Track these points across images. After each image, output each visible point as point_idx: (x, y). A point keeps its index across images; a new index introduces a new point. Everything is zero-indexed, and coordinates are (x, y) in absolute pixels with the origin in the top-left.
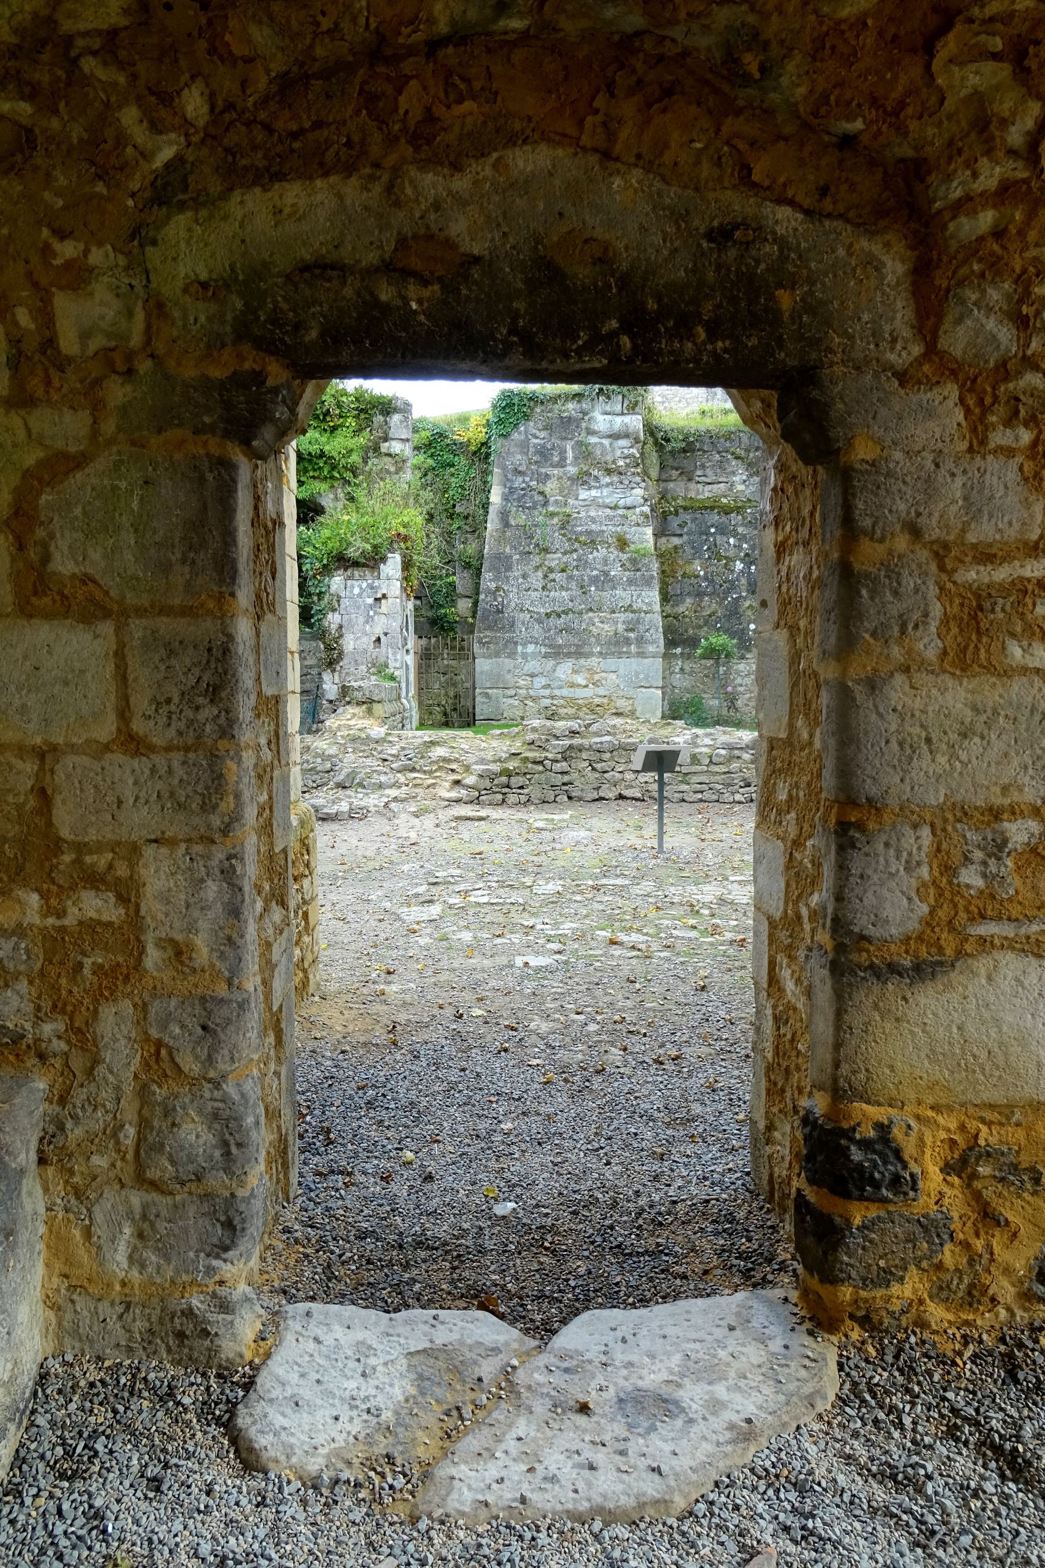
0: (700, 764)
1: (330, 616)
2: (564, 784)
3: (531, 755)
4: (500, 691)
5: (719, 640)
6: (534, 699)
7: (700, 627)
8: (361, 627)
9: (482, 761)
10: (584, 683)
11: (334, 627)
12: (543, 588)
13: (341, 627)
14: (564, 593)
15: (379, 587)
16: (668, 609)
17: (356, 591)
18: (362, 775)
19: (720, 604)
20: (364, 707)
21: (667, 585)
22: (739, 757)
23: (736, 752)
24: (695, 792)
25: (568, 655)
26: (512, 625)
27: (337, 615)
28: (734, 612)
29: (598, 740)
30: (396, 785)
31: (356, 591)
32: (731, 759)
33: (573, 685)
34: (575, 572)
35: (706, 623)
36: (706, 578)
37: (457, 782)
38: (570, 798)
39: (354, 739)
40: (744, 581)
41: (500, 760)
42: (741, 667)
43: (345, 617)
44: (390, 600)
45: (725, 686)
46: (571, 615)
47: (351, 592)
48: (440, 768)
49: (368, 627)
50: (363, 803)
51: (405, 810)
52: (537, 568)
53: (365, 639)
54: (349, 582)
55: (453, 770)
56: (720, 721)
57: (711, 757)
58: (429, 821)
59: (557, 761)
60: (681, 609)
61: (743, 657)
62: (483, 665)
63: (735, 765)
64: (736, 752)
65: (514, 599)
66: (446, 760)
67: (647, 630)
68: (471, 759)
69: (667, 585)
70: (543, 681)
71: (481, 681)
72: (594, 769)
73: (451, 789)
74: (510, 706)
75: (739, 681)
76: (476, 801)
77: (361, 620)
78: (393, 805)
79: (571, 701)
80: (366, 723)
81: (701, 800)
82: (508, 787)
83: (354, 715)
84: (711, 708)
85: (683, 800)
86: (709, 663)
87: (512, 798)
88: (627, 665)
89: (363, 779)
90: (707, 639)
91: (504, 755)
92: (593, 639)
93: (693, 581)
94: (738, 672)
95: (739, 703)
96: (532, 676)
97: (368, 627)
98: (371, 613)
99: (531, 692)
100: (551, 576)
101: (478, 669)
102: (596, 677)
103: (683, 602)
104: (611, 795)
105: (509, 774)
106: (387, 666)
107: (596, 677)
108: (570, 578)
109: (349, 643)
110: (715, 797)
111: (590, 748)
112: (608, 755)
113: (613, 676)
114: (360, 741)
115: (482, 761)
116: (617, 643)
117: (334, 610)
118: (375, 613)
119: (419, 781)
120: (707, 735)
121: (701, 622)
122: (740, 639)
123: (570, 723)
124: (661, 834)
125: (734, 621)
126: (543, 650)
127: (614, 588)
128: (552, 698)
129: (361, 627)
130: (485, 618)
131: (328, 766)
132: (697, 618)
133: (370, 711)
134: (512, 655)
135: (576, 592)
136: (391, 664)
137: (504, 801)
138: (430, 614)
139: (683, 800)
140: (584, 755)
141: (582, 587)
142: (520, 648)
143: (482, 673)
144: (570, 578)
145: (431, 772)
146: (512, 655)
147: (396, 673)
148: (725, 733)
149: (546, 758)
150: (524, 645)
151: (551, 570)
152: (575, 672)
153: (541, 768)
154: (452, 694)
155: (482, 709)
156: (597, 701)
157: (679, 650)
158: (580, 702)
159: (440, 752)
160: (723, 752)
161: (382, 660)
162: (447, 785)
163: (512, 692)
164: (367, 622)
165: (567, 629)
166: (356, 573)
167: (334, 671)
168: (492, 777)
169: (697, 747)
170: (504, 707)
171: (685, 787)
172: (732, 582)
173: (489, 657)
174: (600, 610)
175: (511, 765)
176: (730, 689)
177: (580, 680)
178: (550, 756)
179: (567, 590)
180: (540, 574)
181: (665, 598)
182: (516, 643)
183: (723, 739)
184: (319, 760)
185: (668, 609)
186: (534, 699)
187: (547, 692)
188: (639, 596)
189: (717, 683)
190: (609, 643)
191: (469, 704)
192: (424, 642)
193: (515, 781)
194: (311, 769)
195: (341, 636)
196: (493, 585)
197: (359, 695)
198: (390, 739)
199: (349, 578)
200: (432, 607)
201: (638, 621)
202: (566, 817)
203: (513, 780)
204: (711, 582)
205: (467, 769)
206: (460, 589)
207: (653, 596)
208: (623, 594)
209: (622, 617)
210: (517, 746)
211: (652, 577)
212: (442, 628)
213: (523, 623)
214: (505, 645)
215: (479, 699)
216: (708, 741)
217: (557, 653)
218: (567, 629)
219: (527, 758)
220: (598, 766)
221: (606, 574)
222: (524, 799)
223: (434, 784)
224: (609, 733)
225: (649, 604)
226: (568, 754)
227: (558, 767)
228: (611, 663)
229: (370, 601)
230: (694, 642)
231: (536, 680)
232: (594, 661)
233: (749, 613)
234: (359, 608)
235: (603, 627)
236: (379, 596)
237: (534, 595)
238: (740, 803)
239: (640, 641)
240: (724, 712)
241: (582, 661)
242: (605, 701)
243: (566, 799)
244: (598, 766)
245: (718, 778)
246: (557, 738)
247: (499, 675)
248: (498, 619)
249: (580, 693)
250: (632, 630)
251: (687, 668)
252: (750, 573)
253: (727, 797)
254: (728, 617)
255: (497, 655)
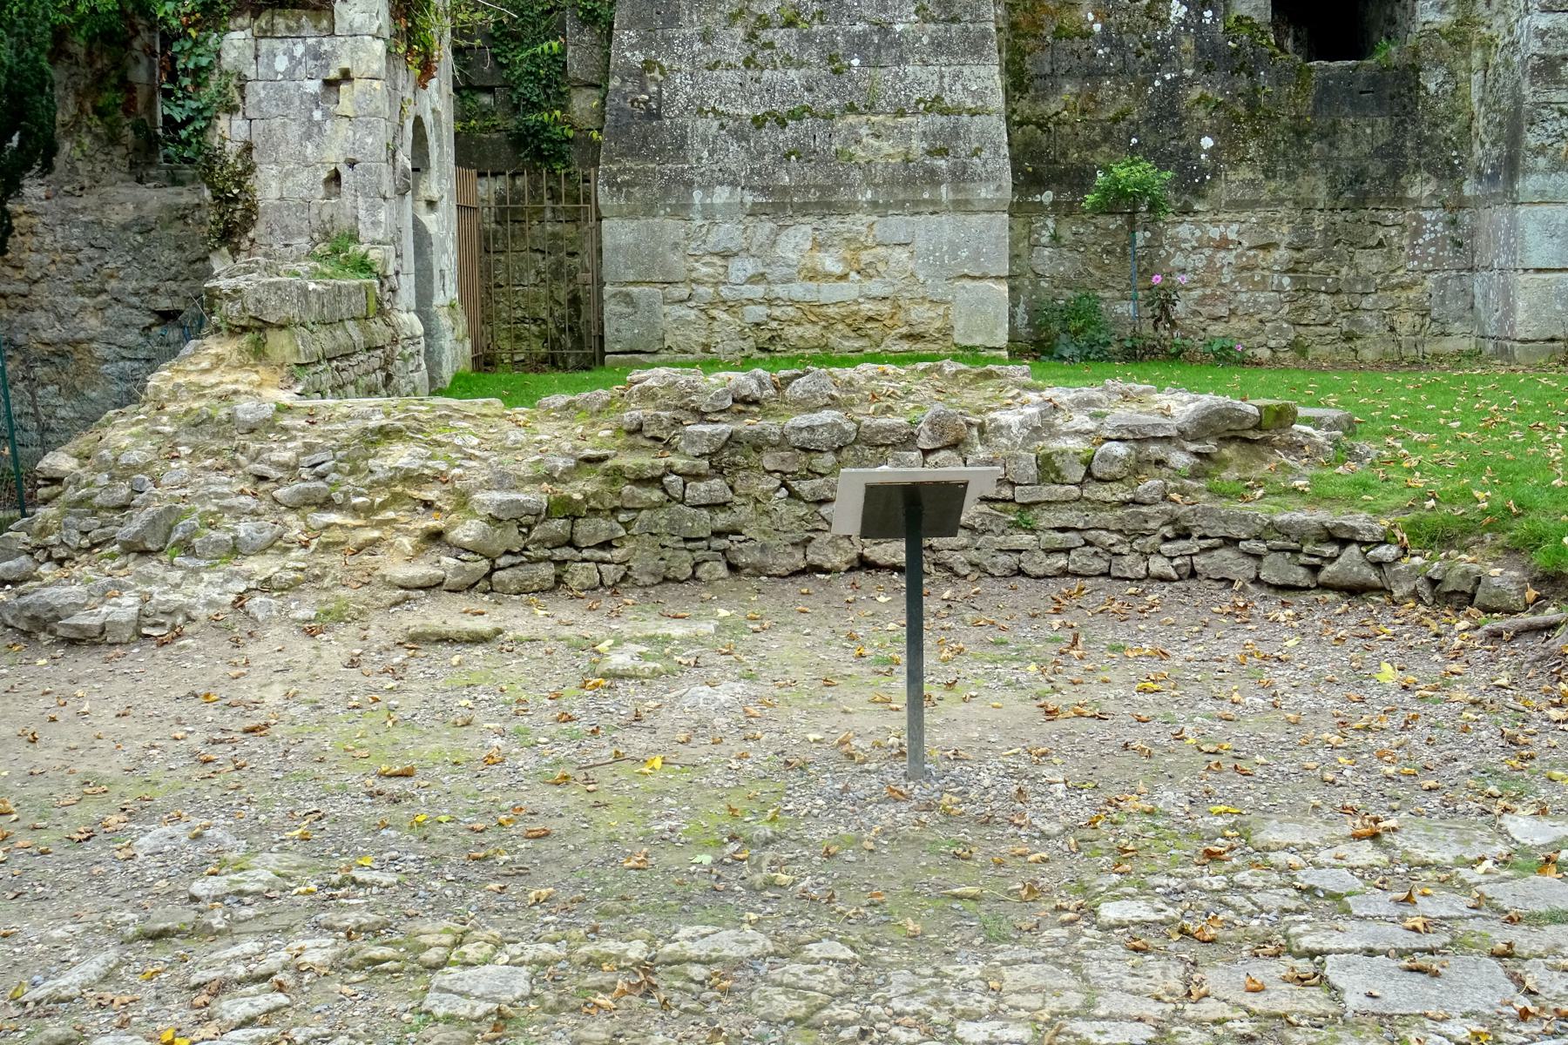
0: (1059, 479)
1: (223, 123)
2: (718, 534)
3: (629, 461)
4: (657, 290)
5: (1130, 172)
6: (731, 307)
7: (1093, 146)
8: (294, 147)
9: (501, 481)
10: (838, 269)
11: (232, 148)
12: (748, 63)
13: (248, 148)
14: (792, 73)
15: (333, 54)
16: (1024, 107)
17: (281, 64)
18: (192, 521)
19: (1137, 94)
20: (248, 337)
21: (1023, 54)
22: (1160, 463)
23: (1154, 450)
24: (1050, 552)
25: (804, 209)
26: (681, 144)
27: (238, 121)
28: (1167, 112)
29: (802, 420)
30: (276, 545)
31: (281, 64)
32: (1137, 468)
33: (814, 275)
34: (817, 27)
35: (1107, 136)
36: (1105, 39)
37: (435, 537)
38: (733, 568)
39: (198, 423)
40: (1188, 43)
41: (550, 478)
42: (1184, 230)
43: (259, 125)
44: (358, 84)
45: (1146, 273)
46: (808, 122)
47: (270, 66)
48: (396, 499)
49: (310, 149)
50: (177, 598)
51: (284, 616)
52: (733, 18)
53: (304, 177)
54: (264, 44)
55: (428, 505)
56: (1137, 354)
57: (1088, 463)
58: (336, 647)
59: (698, 477)
60: (1052, 106)
61: (1186, 210)
62: (618, 233)
63: (1150, 484)
64: (1154, 450)
65: (683, 86)
66: (411, 478)
67: (975, 153)
68: (476, 472)
69: (1023, 54)
70: (751, 266)
71: (613, 266)
72: (793, 495)
73: (418, 552)
74: (678, 321)
75: (1178, 260)
76: (484, 584)
77: (295, 130)
78: (256, 602)
79: (810, 311)
80: (244, 379)
81: (1065, 572)
82: (571, 543)
83: (220, 359)
84: (1117, 321)
85: (1020, 572)
86: (1114, 223)
87: (581, 574)
88: (935, 231)
89: (194, 532)
90: (1107, 170)
91: (561, 463)
92: (857, 175)
93: (1078, 44)
94: (1176, 243)
95: (1180, 309)
96: (726, 255)
97: (310, 149)
98: (317, 115)
99: (725, 291)
100: (765, 35)
101: (607, 241)
102: (865, 257)
103: (1057, 90)
104: (838, 560)
105: (569, 510)
106: (354, 238)
107: (865, 257)
108: (806, 38)
109: (268, 186)
110: (1099, 565)
111: (782, 443)
112: (829, 459)
113: (901, 254)
114: (214, 430)
115: (501, 481)
116: (909, 182)
117: (232, 110)
118: (327, 115)
119: (337, 535)
120: (1082, 404)
121: (1096, 135)
122: (1181, 169)
123: (737, 377)
124: (917, 699)
125: (1167, 130)
126: (749, 199)
127: (902, 60)
128: (770, 303)
129: (294, 147)
130: (620, 130)
131: (123, 491)
132: (1088, 126)
133: (259, 352)
134: (682, 210)
135: (819, 71)
136: (366, 234)
137: (559, 580)
138: (512, 123)
139: (1020, 572)
140: (769, 461)
141: (832, 59)
142: (697, 195)
143: (616, 249)
144: (806, 38)
145: (370, 510)
146: (682, 210)
147: (374, 255)
148: (1126, 396)
149: (670, 470)
150: (707, 188)
151: (764, 22)
152: (818, 245)
153: (656, 495)
154: (563, 295)
155: (618, 327)
156: (868, 308)
157: (1048, 197)
158: (831, 311)
159: (400, 456)
160: (1120, 450)
161: (344, 223)
162: (407, 543)
163: (682, 291)
164: (309, 137)
165: (800, 153)
166: (280, 22)
167: (235, 251)
168: (524, 521)
169: (1055, 436)
170: (664, 323)
171: (1024, 539)
172: (1162, 47)
173: (632, 215)
174: (870, 108)
175: (576, 491)
176: (1157, 280)
177: (830, 262)
178: (680, 463)
179: (800, 65)
180: (739, 32)
181: (1017, 82)
182: (689, 185)
183: (1123, 414)
184: (103, 479)
185: (1024, 107)
186: (731, 307)
187: (759, 291)
188: (957, 76)
189: (1131, 266)
190: (892, 182)
191: (593, 317)
192: (488, 189)
193: (587, 529)
194: (80, 502)
195: (250, 169)
196: (638, 58)
197: (230, 309)
198: (287, 421)
199: (264, 34)
200: (516, 108)
201: (955, 133)
202: (707, 628)
203: (584, 529)
204: (1119, 47)
205: (463, 500)
206: (575, 69)
207: (988, 77)
208: (923, 74)
209: (920, 123)
210: (600, 438)
211: (985, 35)
212: (538, 154)
213: (704, 141)
214: (666, 191)
215: (610, 308)
216: (1082, 421)
217: (778, 206)
218: (800, 153)
219: (618, 470)
220: (805, 487)
221: (884, 29)
222: (611, 573)
223: (373, 543)
224: (833, 403)
225: (979, 95)
226: (724, 459)
227: (700, 491)
228: (897, 226)
229: (314, 86)
230: (1079, 179)
231: (735, 264)
232: (859, 223)
233: (1201, 113)
234: (288, 103)
235: (879, 145)
236: (334, 74)
237: (728, 77)
238: (1162, 579)
239: (961, 176)
240: (1147, 329)
241: (834, 223)
242: (886, 308)
243: (722, 570)
244: (805, 487)
245: (1107, 516)
246: (701, 416)
247: (653, 256)
248: (647, 130)
249: (829, 292)
250: (942, 152)
251: (1066, 234)
252: (1200, 27)
253: (1131, 564)
254: (1154, 123)
255: (650, 211)
